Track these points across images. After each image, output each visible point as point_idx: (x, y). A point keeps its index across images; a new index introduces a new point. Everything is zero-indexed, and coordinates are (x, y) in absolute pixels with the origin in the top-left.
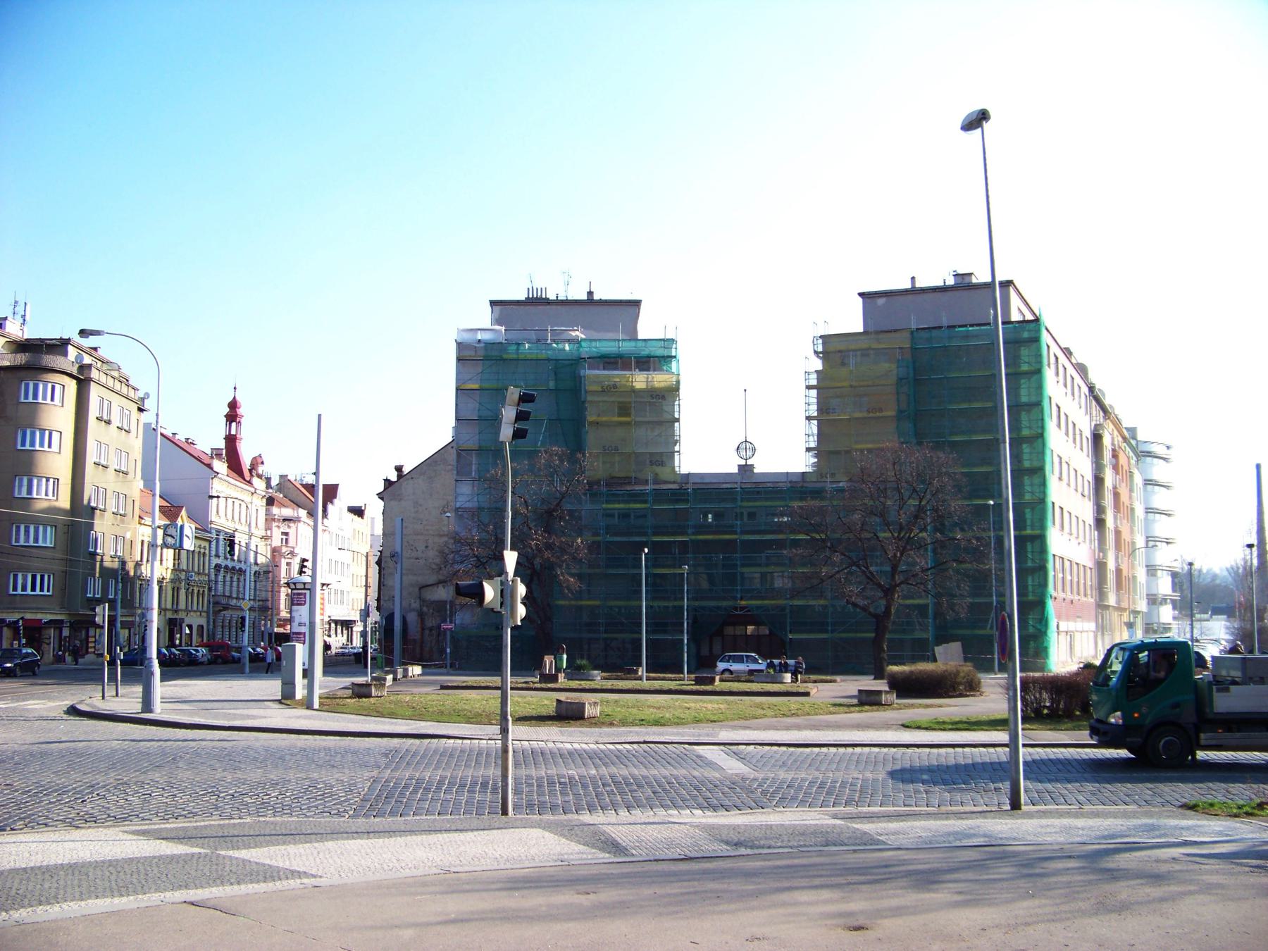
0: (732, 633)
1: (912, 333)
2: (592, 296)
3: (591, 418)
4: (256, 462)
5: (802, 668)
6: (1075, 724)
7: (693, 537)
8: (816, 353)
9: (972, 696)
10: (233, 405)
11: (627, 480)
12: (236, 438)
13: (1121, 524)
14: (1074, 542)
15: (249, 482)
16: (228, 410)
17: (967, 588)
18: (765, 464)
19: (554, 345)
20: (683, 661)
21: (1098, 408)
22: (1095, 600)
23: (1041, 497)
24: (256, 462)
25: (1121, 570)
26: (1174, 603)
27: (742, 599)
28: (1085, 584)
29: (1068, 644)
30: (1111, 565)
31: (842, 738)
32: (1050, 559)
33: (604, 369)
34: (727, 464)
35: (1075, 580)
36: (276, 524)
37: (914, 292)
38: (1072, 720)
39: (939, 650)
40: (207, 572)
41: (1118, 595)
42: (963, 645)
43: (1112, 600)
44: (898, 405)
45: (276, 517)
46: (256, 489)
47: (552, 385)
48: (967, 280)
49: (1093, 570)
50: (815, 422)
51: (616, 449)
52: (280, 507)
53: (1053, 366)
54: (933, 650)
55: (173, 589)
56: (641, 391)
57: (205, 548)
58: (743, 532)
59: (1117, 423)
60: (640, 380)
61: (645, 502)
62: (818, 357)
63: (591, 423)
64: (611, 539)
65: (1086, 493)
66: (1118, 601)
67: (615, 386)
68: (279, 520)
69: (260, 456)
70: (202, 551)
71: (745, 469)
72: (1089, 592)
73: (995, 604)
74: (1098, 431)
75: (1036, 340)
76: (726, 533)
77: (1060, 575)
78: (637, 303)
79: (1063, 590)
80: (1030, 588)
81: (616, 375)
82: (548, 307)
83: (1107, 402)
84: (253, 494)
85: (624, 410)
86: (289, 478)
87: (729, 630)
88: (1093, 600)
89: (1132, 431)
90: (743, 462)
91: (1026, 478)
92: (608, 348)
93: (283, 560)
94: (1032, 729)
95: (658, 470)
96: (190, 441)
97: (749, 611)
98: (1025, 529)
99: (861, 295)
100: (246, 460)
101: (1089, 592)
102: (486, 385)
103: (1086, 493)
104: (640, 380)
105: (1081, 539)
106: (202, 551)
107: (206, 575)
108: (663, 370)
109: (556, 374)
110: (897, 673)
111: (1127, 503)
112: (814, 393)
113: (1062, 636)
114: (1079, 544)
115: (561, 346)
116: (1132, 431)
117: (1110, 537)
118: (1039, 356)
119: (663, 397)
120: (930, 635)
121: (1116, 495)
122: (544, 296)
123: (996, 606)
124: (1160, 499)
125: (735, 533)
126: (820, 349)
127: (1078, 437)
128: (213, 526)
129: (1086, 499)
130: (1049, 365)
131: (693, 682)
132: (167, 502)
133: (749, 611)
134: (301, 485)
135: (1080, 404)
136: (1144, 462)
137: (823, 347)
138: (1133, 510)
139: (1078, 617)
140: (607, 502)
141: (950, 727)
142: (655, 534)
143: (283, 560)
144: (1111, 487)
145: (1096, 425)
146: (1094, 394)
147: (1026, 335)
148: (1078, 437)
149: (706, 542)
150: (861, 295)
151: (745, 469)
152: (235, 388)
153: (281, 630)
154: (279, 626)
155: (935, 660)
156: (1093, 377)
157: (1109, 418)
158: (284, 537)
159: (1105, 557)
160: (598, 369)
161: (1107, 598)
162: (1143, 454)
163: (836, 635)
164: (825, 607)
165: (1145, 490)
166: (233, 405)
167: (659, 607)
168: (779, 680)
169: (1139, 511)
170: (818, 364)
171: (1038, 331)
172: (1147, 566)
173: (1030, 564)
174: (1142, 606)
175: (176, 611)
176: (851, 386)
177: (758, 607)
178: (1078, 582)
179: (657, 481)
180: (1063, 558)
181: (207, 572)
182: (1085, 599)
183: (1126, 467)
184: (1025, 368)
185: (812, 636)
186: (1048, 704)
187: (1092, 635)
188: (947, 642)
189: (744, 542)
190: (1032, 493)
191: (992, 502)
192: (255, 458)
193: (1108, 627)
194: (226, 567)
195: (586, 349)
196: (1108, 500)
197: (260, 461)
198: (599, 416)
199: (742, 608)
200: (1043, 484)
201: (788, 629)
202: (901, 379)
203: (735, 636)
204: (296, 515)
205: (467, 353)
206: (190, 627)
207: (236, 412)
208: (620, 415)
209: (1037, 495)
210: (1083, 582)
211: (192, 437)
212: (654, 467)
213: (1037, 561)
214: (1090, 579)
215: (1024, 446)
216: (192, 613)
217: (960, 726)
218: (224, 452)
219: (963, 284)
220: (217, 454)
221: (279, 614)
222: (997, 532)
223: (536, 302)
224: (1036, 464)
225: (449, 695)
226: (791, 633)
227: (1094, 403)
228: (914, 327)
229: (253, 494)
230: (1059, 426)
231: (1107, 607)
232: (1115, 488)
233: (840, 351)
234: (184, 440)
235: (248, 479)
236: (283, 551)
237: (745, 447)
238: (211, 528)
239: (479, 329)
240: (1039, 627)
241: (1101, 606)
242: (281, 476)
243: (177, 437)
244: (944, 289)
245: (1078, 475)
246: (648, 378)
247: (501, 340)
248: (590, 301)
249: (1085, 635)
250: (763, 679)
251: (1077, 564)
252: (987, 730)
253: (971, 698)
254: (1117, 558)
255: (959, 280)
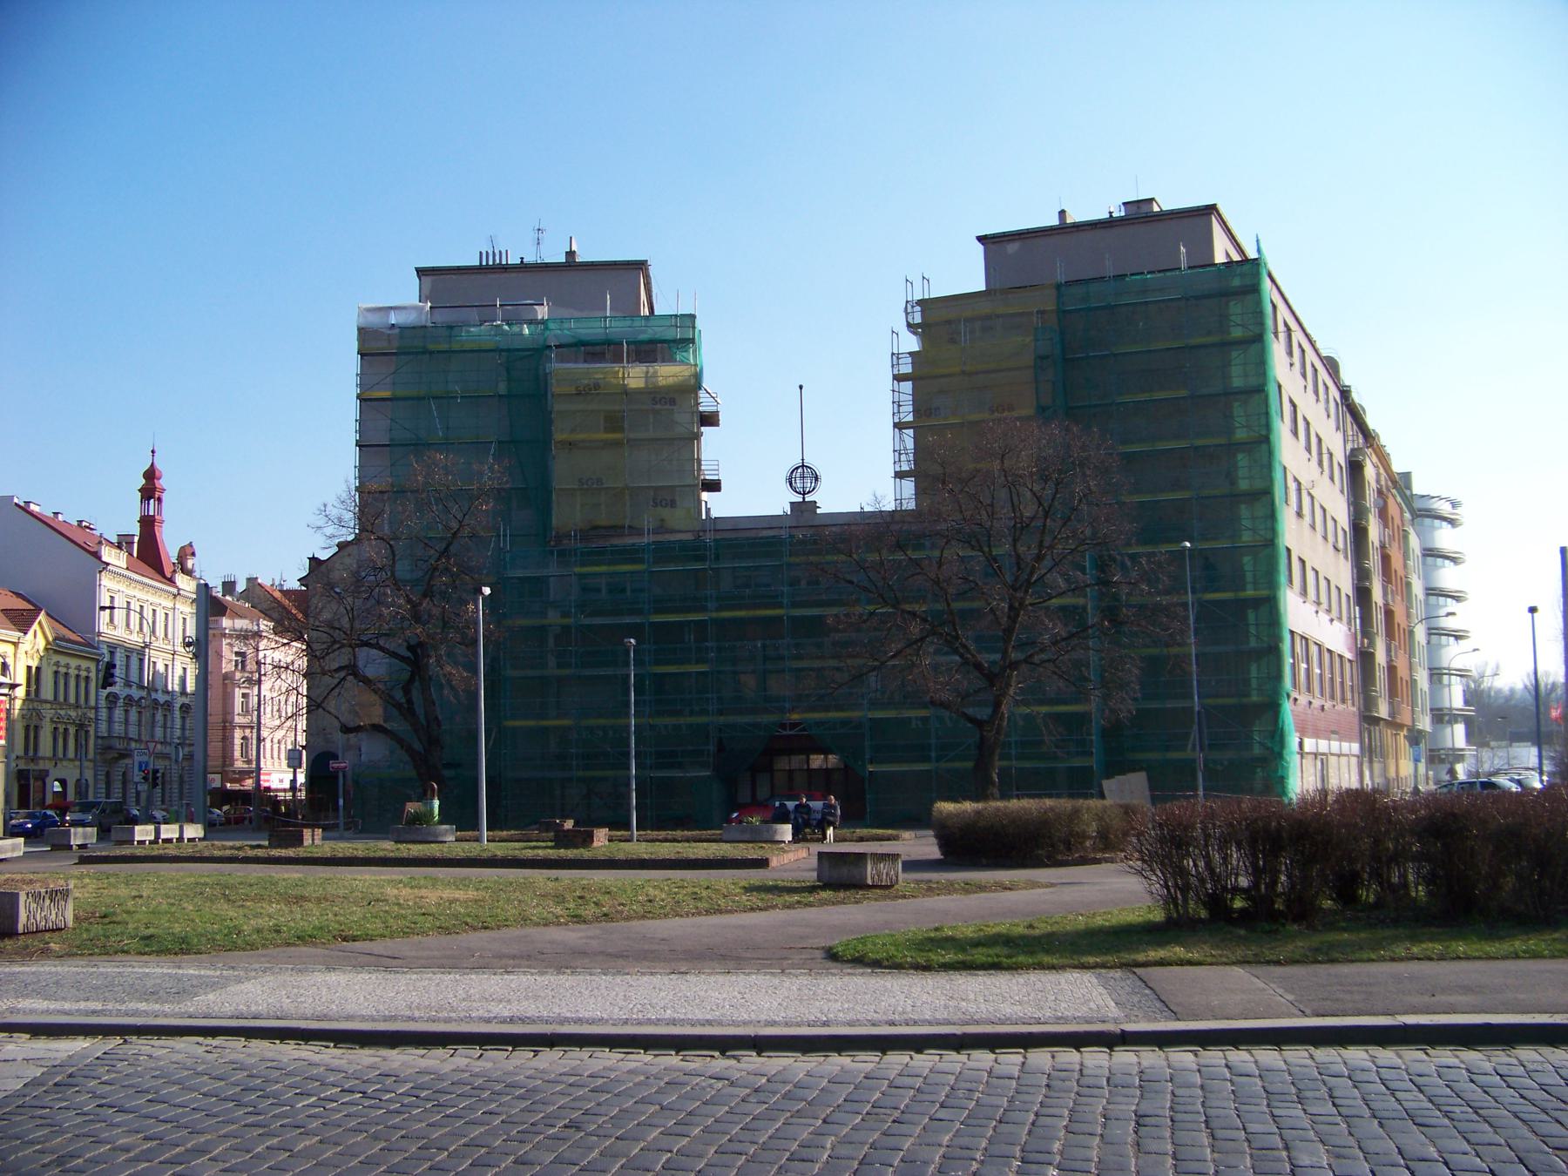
0: (787, 768)
1: (1058, 287)
2: (574, 258)
3: (558, 436)
4: (186, 552)
5: (834, 815)
6: (1316, 940)
7: (714, 615)
8: (909, 325)
9: (1106, 860)
10: (151, 475)
11: (616, 530)
12: (154, 521)
13: (1393, 601)
14: (1324, 617)
15: (171, 581)
16: (144, 481)
17: (1136, 671)
18: (833, 499)
19: (506, 327)
20: (629, 804)
21: (1355, 427)
22: (1359, 709)
23: (1269, 536)
24: (186, 552)
25: (1395, 667)
26: (1468, 721)
27: (792, 710)
28: (1342, 683)
29: (1319, 774)
30: (1381, 657)
31: (531, 1009)
32: (1287, 637)
33: (585, 361)
34: (774, 501)
35: (1327, 675)
36: (228, 641)
37: (1065, 229)
38: (1312, 928)
39: (1107, 785)
40: (92, 703)
41: (1391, 704)
42: (1150, 779)
43: (1383, 711)
44: (1038, 399)
45: (227, 631)
46: (179, 589)
47: (502, 388)
48: (1144, 209)
49: (1354, 664)
50: (911, 432)
51: (599, 481)
52: (232, 618)
53: (1282, 336)
54: (1100, 786)
55: (27, 728)
56: (638, 391)
57: (88, 670)
58: (794, 605)
59: (1384, 459)
60: (635, 376)
61: (641, 561)
62: (914, 333)
63: (562, 442)
64: (587, 621)
65: (1341, 545)
66: (1392, 713)
67: (597, 386)
68: (231, 636)
69: (190, 545)
70: (84, 674)
71: (804, 509)
72: (1349, 695)
73: (1197, 709)
74: (1355, 456)
75: (1254, 289)
76: (766, 606)
77: (1304, 666)
78: (641, 266)
79: (1309, 689)
80: (1254, 683)
81: (600, 370)
82: (506, 275)
83: (1372, 422)
84: (175, 596)
85: (614, 422)
86: (259, 581)
87: (782, 764)
88: (1355, 709)
89: (1407, 476)
90: (799, 499)
91: (1243, 506)
92: (591, 329)
93: (237, 690)
94: (1190, 963)
95: (665, 513)
96: (84, 524)
97: (804, 729)
98: (1244, 589)
99: (980, 239)
100: (170, 547)
101: (1349, 695)
102: (400, 393)
103: (1341, 545)
104: (635, 376)
105: (1335, 613)
106: (84, 674)
107: (91, 708)
108: (676, 361)
109: (508, 370)
110: (950, 815)
111: (1401, 573)
112: (907, 386)
113: (1308, 761)
114: (1332, 620)
115: (516, 329)
116: (1407, 476)
117: (1378, 618)
118: (1260, 314)
119: (673, 402)
120: (1094, 762)
121: (1386, 559)
122: (504, 262)
123: (1199, 712)
124: (1448, 577)
125: (780, 606)
126: (918, 319)
127: (1325, 458)
128: (101, 638)
129: (1341, 556)
130: (1276, 334)
131: (553, 844)
132: (29, 602)
133: (804, 729)
134: (281, 591)
135: (1327, 410)
136: (1422, 525)
137: (923, 316)
138: (1409, 585)
139: (1333, 732)
140: (583, 565)
141: (950, 957)
142: (658, 611)
143: (237, 690)
144: (1377, 544)
145: (1353, 450)
146: (1351, 411)
147: (1236, 282)
148: (1325, 458)
149: (734, 620)
150: (980, 239)
151: (804, 509)
152: (153, 452)
153: (237, 787)
154: (233, 781)
155: (1102, 796)
156: (1347, 378)
157: (1371, 446)
158: (239, 659)
159: (1372, 644)
160: (576, 362)
161: (1376, 705)
162: (1423, 513)
163: (944, 765)
164: (925, 720)
165: (1424, 563)
166: (151, 475)
167: (666, 726)
168: (766, 836)
169: (1418, 588)
170: (911, 343)
171: (1256, 275)
172: (1430, 669)
173: (1253, 643)
174: (1425, 723)
175: (32, 760)
176: (963, 372)
177: (819, 723)
178: (1332, 679)
179: (661, 528)
180: (1307, 639)
181: (92, 703)
182: (1340, 707)
183: (1397, 521)
184: (1237, 333)
185: (905, 767)
186: (1244, 882)
187: (1354, 760)
188: (1123, 772)
189: (793, 619)
190: (1254, 530)
191: (1188, 544)
192: (182, 548)
193: (1378, 750)
194: (129, 698)
195: (556, 334)
196: (1374, 562)
197: (189, 551)
198: (573, 431)
199: (794, 725)
200: (1272, 516)
201: (867, 757)
202: (1042, 358)
203: (791, 772)
204: (256, 628)
205: (381, 345)
206: (63, 783)
207: (154, 484)
208: (607, 430)
209: (1262, 533)
210: (1339, 680)
211: (87, 519)
212: (659, 508)
213: (1265, 639)
214: (1350, 676)
215: (1240, 456)
216: (65, 763)
217: (979, 955)
218: (136, 539)
219: (1140, 214)
220: (123, 543)
221: (232, 765)
222: (1200, 595)
223: (492, 270)
224: (1259, 484)
225: (178, 870)
226: (871, 763)
227: (1349, 418)
228: (1061, 279)
229: (175, 596)
230: (1295, 433)
231: (1377, 720)
232: (1383, 547)
233: (949, 322)
234: (76, 524)
235: (169, 576)
236: (237, 678)
237: (803, 476)
238: (99, 641)
239: (391, 308)
240: (1270, 745)
241: (1368, 719)
242: (249, 580)
243: (60, 517)
244: (1109, 223)
245: (1328, 518)
246: (647, 372)
247: (423, 323)
248: (570, 264)
249: (1344, 760)
250: (738, 836)
251: (1330, 651)
252: (1052, 967)
253: (1104, 866)
254: (1389, 650)
255: (1133, 209)
